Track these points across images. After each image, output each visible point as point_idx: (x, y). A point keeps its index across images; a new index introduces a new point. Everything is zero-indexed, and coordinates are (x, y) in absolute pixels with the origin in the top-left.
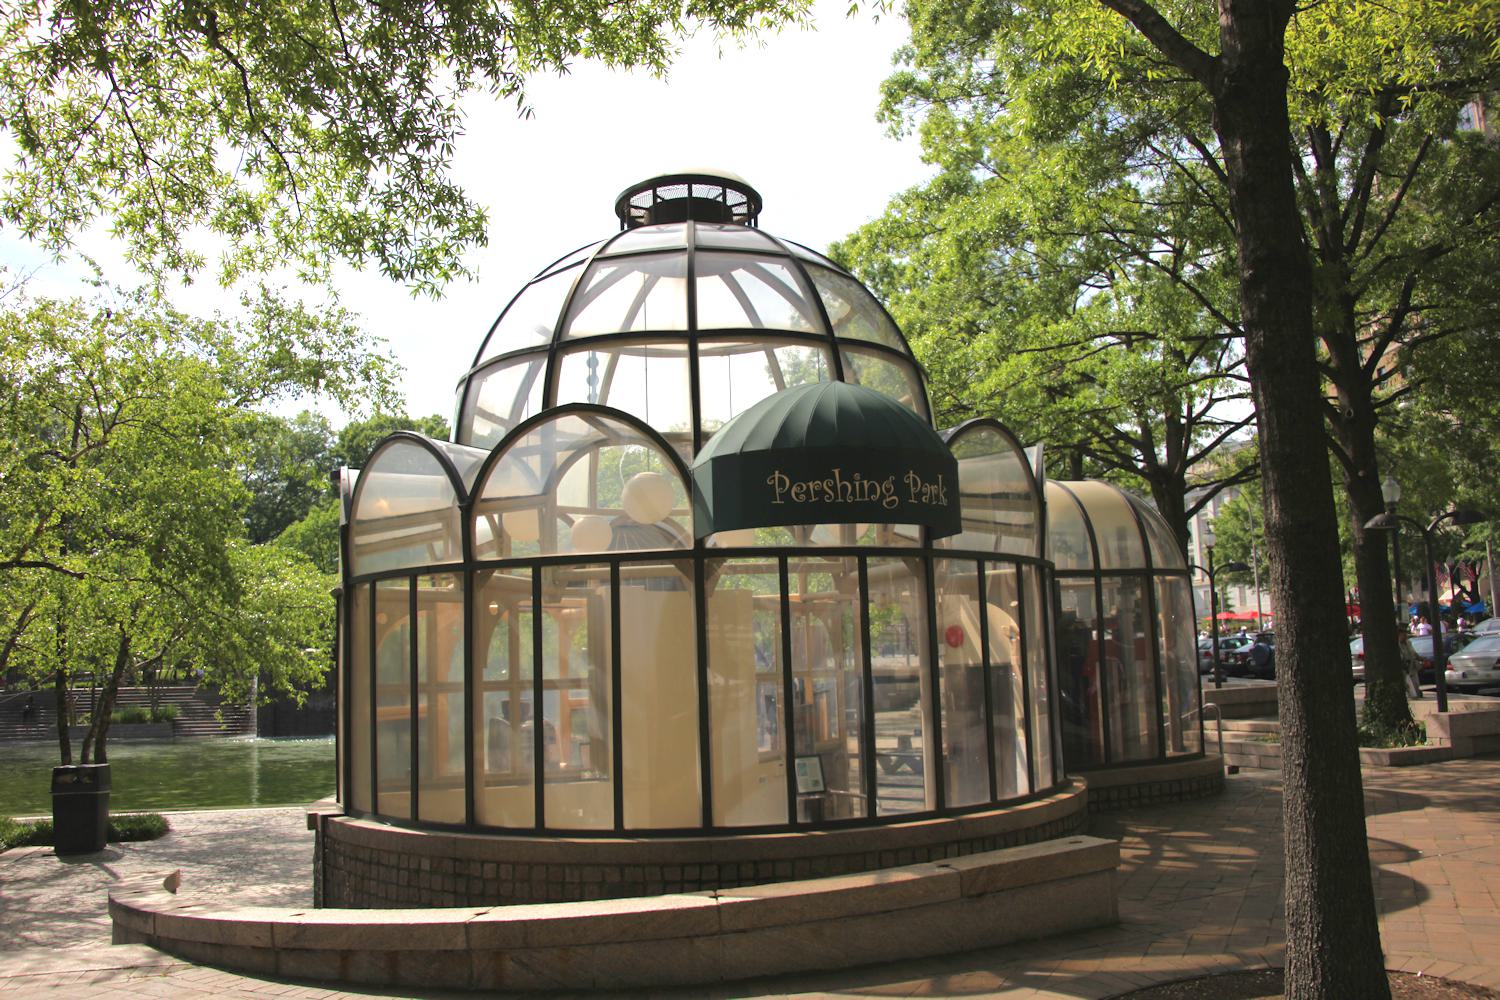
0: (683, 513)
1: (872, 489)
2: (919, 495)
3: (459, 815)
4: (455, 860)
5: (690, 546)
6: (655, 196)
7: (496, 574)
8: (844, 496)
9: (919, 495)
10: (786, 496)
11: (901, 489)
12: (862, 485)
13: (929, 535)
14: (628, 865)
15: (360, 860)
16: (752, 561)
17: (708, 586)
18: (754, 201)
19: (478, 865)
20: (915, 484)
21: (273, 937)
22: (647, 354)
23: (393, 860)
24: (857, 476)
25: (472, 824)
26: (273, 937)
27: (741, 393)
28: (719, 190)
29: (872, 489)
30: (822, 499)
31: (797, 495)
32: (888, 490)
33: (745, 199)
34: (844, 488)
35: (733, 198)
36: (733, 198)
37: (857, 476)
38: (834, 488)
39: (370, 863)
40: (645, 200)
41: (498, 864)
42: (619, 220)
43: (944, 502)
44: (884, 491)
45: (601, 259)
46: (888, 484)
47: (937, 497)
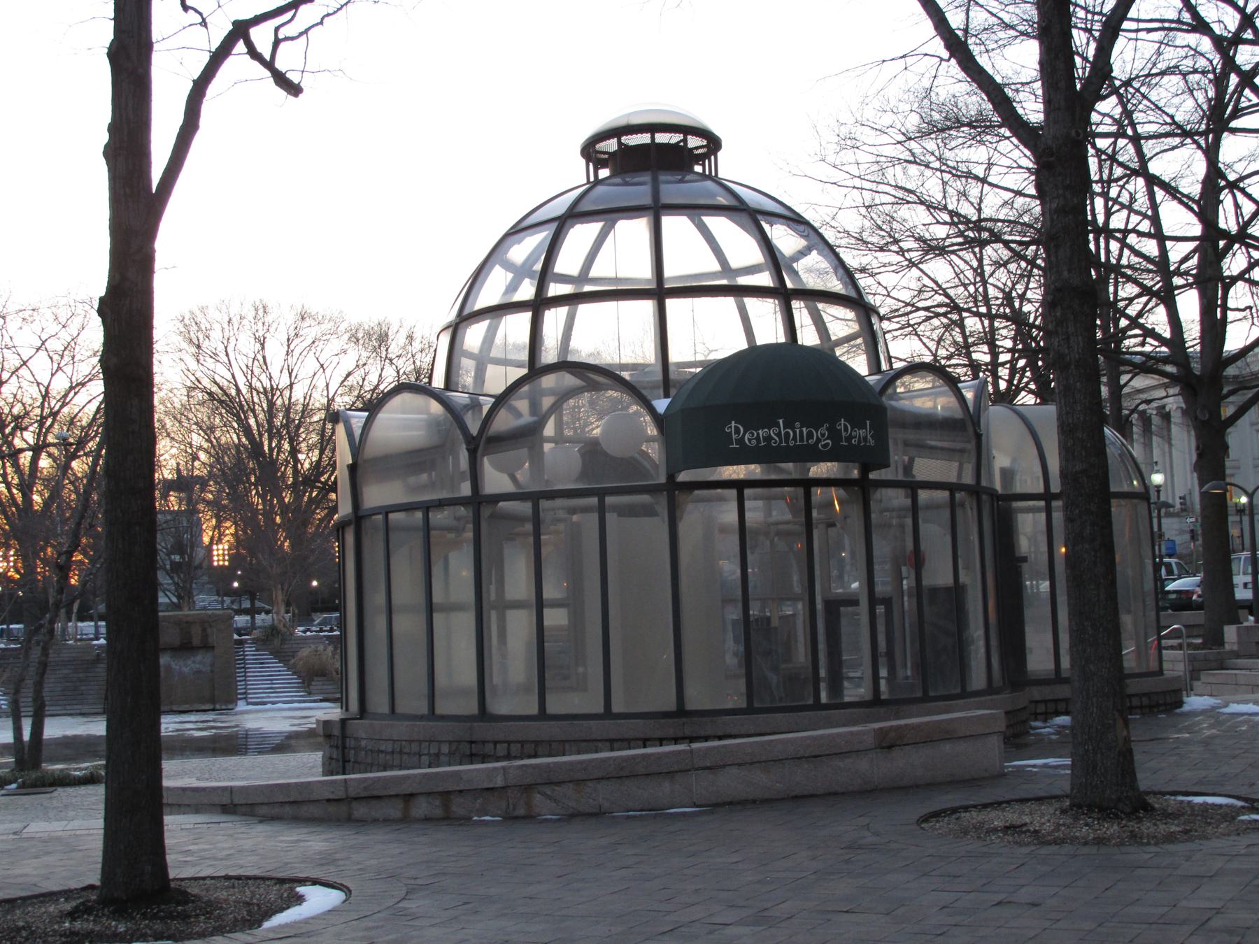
0: (650, 440)
1: (810, 435)
2: (849, 439)
3: (472, 707)
4: (471, 742)
5: (662, 479)
6: (620, 143)
7: (501, 504)
8: (787, 441)
9: (849, 439)
10: (741, 441)
11: (834, 434)
12: (801, 432)
13: (865, 470)
14: (617, 740)
15: (1124, 106)
16: (1031, 503)
17: (678, 514)
18: (714, 144)
19: (491, 746)
20: (846, 430)
21: (346, 790)
22: (617, 280)
23: (415, 747)
24: (798, 424)
25: (484, 714)
26: (346, 790)
27: (709, 334)
28: (681, 137)
29: (810, 435)
30: (769, 445)
31: (750, 440)
32: (823, 435)
33: (705, 143)
34: (787, 434)
35: (693, 142)
36: (693, 142)
37: (798, 424)
38: (779, 435)
39: (393, 753)
40: (611, 145)
41: (509, 743)
42: (583, 162)
43: (872, 442)
44: (820, 436)
45: (575, 215)
46: (823, 430)
47: (865, 439)
